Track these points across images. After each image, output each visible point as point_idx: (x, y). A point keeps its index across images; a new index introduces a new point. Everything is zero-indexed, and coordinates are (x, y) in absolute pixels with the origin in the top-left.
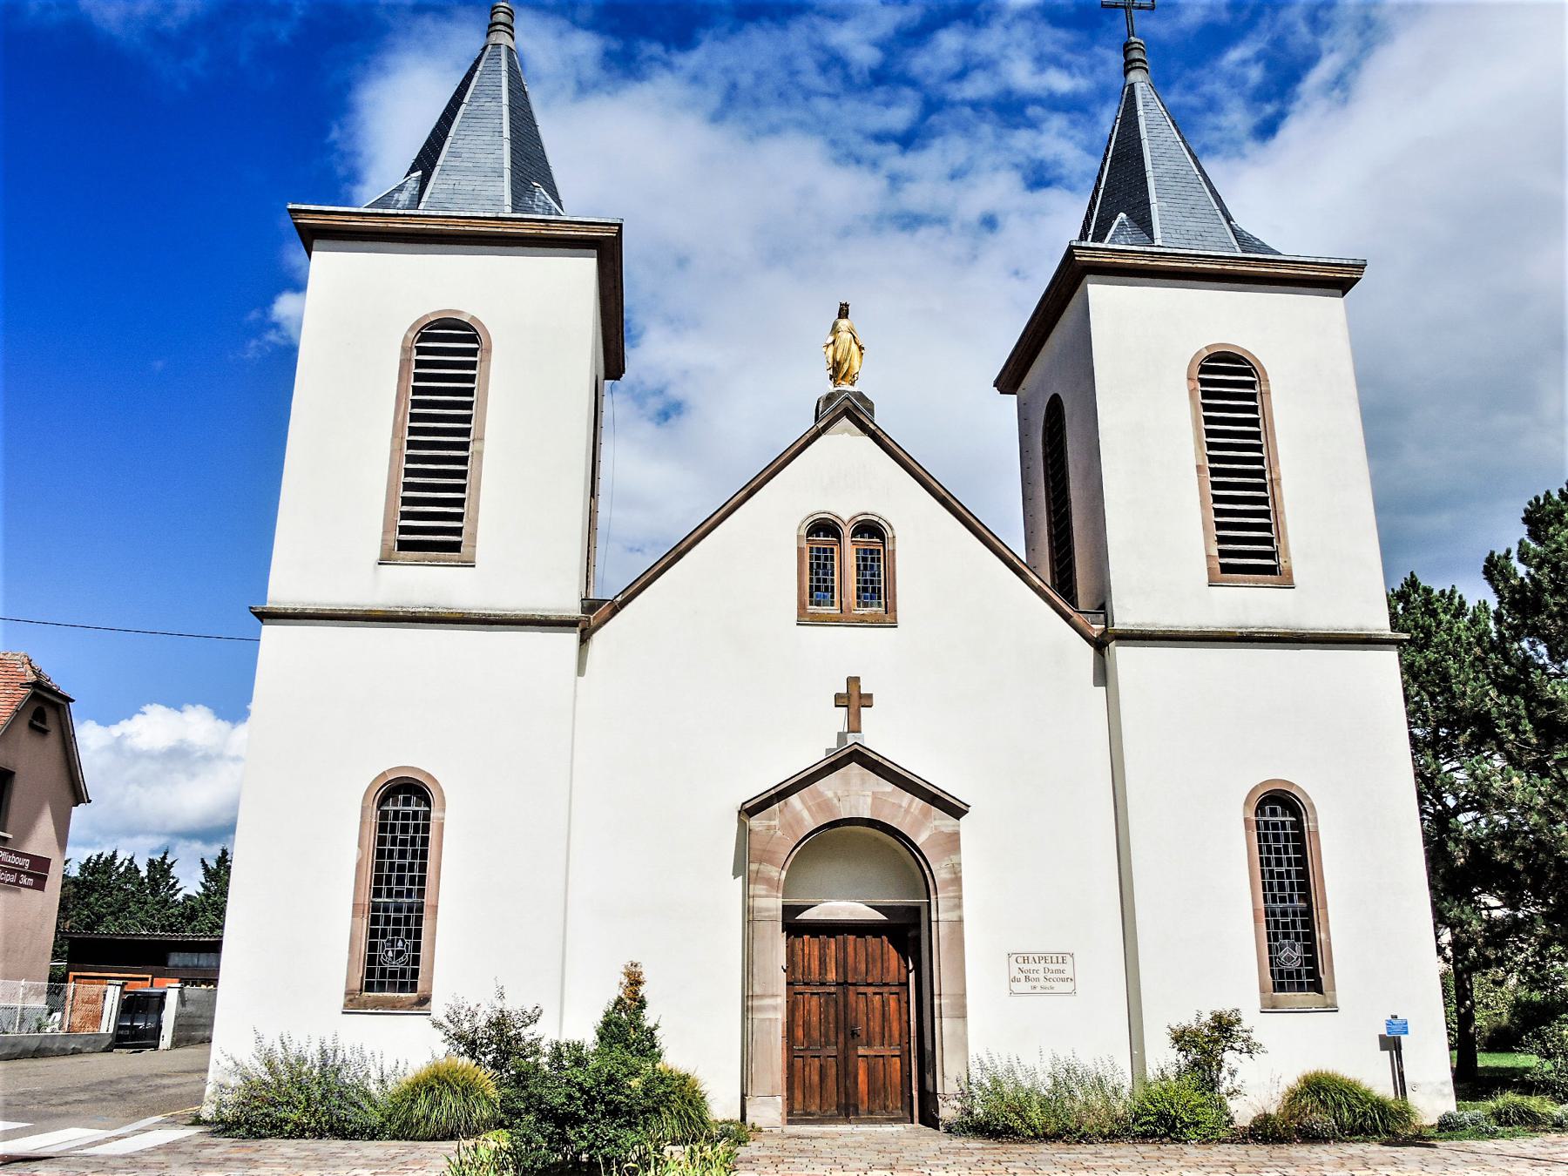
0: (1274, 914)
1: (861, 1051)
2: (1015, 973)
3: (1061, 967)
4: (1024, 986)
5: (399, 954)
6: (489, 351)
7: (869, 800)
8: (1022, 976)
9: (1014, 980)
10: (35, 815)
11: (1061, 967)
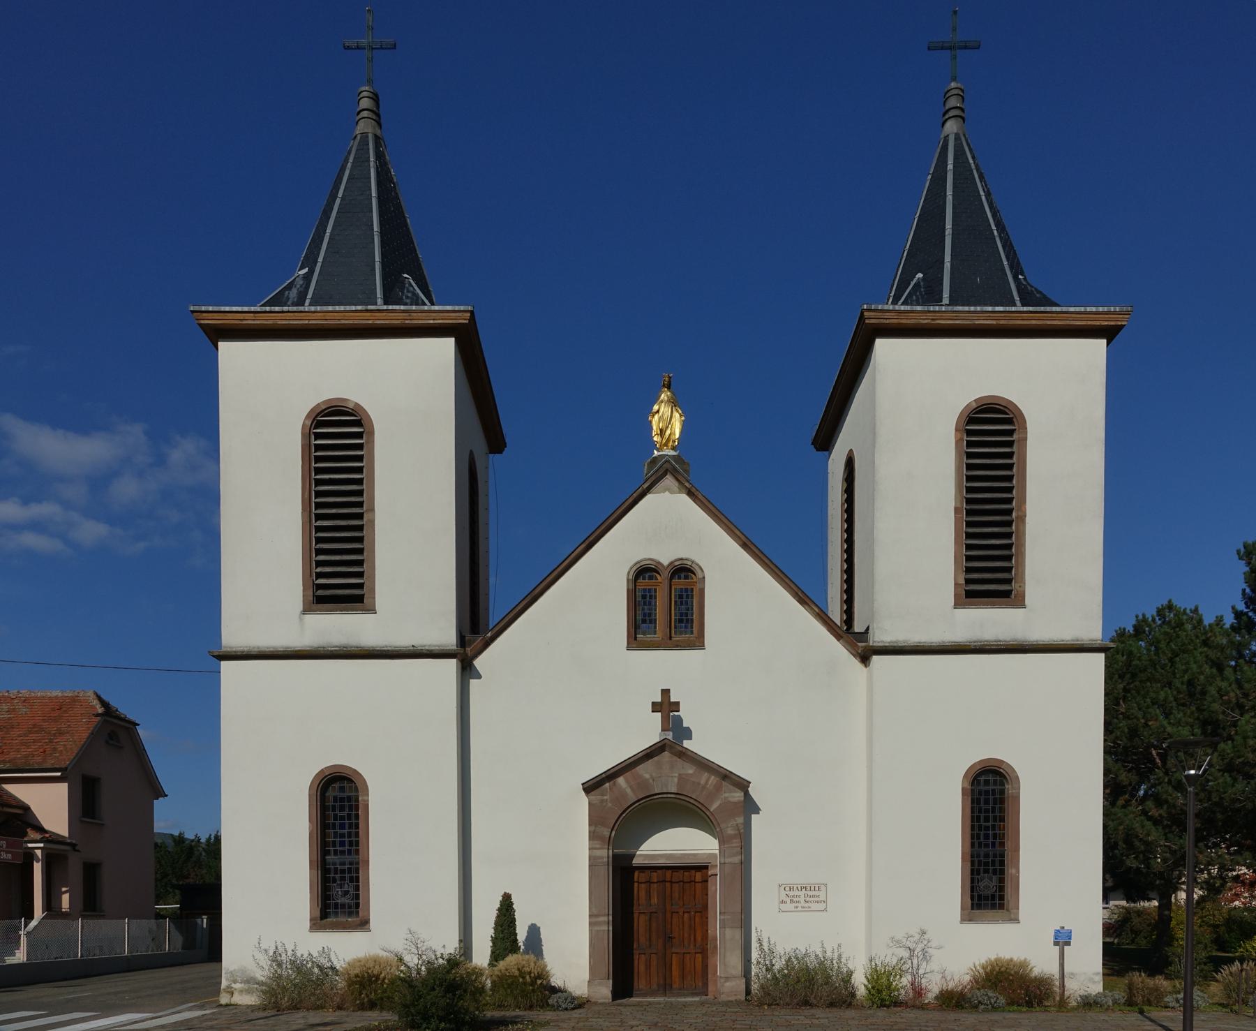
0: (978, 856)
1: (674, 950)
2: (783, 897)
3: (817, 893)
4: (790, 906)
5: (346, 893)
6: (372, 433)
7: (676, 780)
8: (788, 900)
9: (782, 902)
10: (4, 790)
11: (817, 893)
